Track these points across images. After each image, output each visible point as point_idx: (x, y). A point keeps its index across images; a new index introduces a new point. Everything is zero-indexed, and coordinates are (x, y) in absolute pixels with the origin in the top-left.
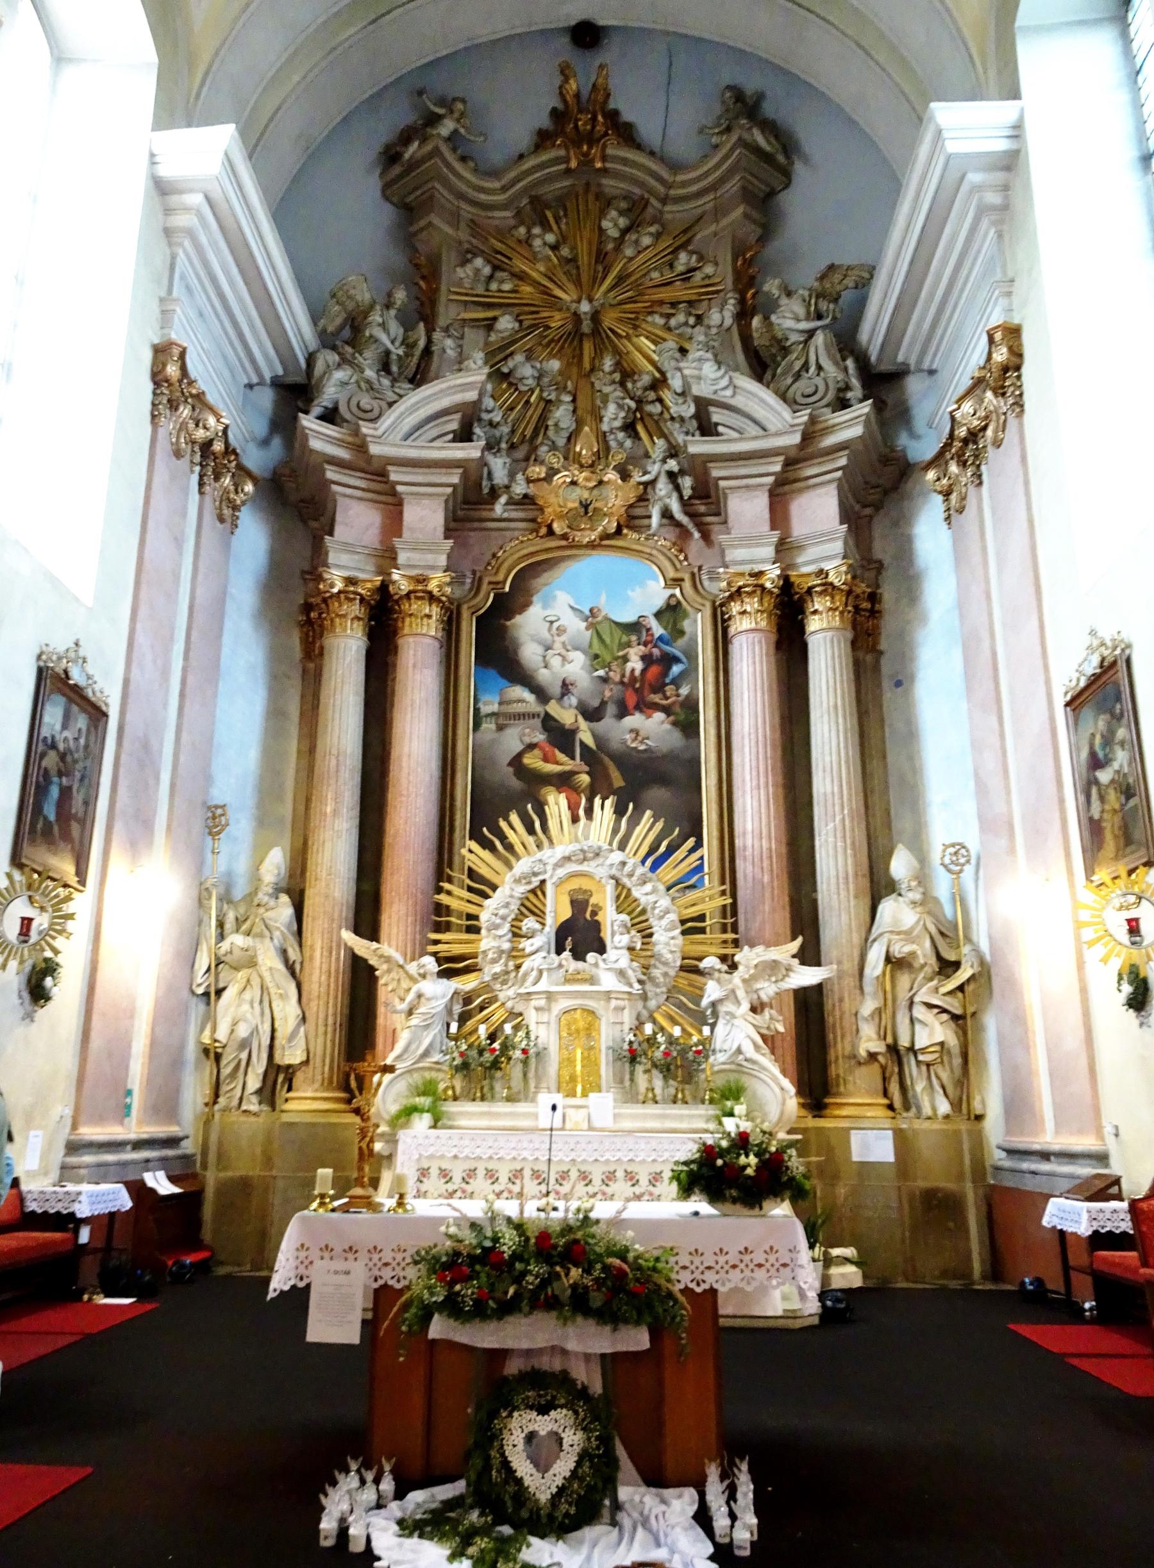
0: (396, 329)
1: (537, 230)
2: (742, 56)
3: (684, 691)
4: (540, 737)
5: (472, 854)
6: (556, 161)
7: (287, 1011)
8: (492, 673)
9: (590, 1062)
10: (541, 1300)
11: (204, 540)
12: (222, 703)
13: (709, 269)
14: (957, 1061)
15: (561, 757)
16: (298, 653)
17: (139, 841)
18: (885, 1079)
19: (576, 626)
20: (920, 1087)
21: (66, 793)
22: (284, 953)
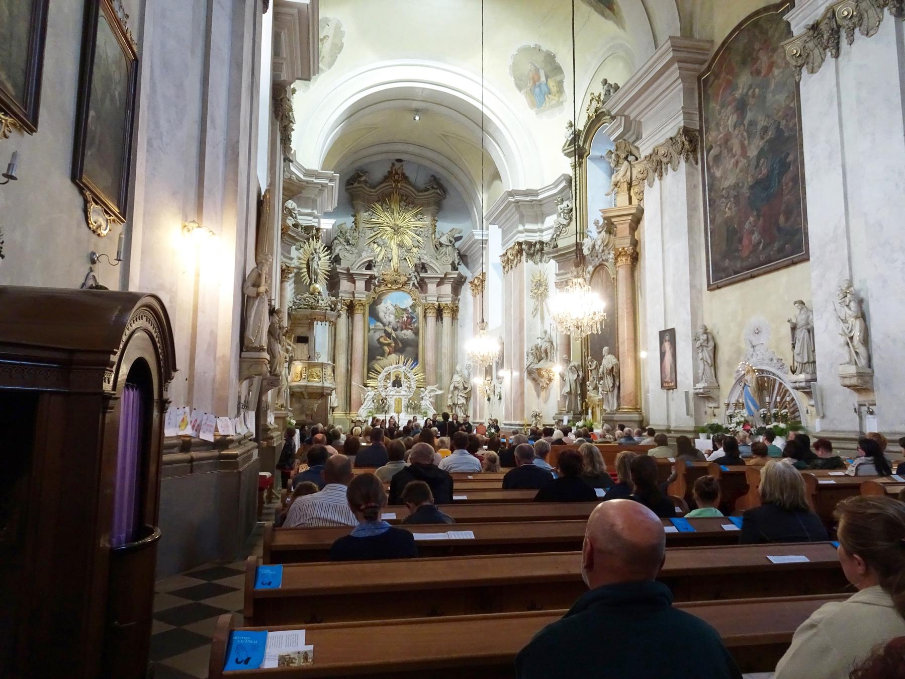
19: (392, 309)
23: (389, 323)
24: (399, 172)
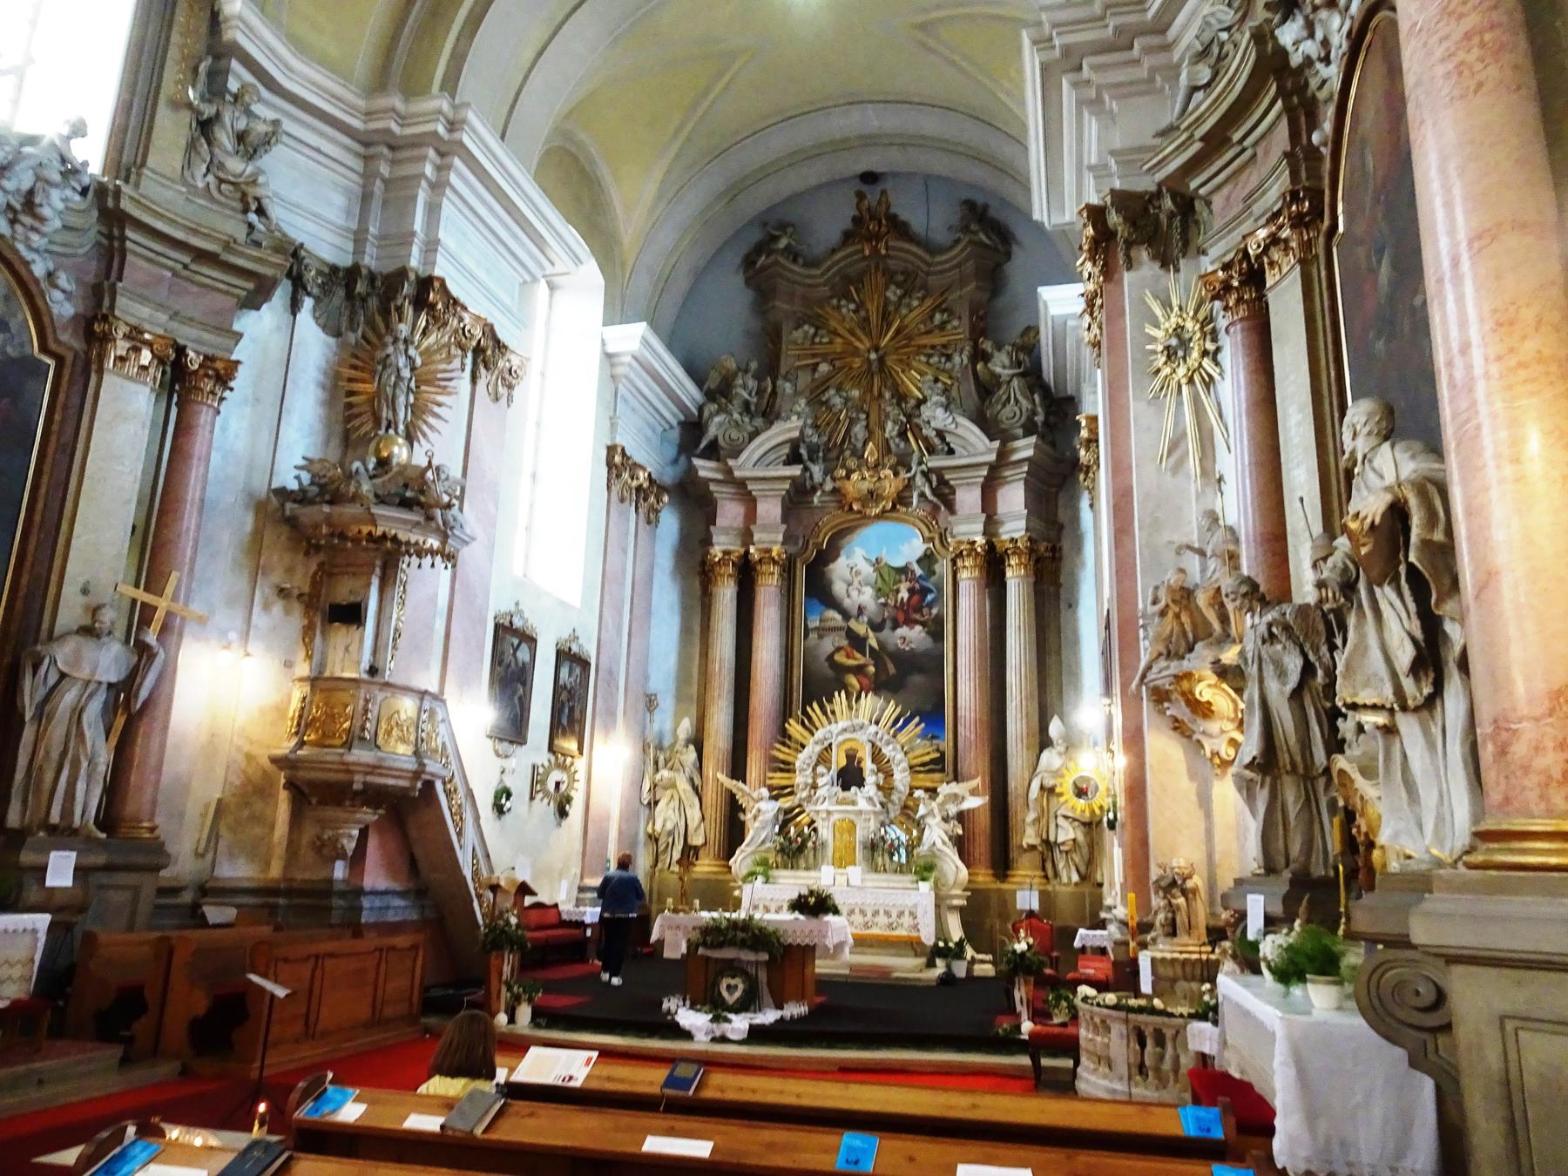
0: (752, 383)
1: (843, 302)
2: (972, 186)
3: (935, 611)
4: (845, 643)
6: (856, 252)
7: (694, 814)
8: (815, 601)
10: (732, 943)
11: (640, 543)
12: (654, 631)
13: (956, 323)
14: (1085, 850)
15: (858, 655)
16: (699, 593)
17: (609, 726)
18: (1044, 861)
19: (867, 570)
20: (1061, 865)
21: (572, 710)
22: (692, 780)
23: (861, 610)
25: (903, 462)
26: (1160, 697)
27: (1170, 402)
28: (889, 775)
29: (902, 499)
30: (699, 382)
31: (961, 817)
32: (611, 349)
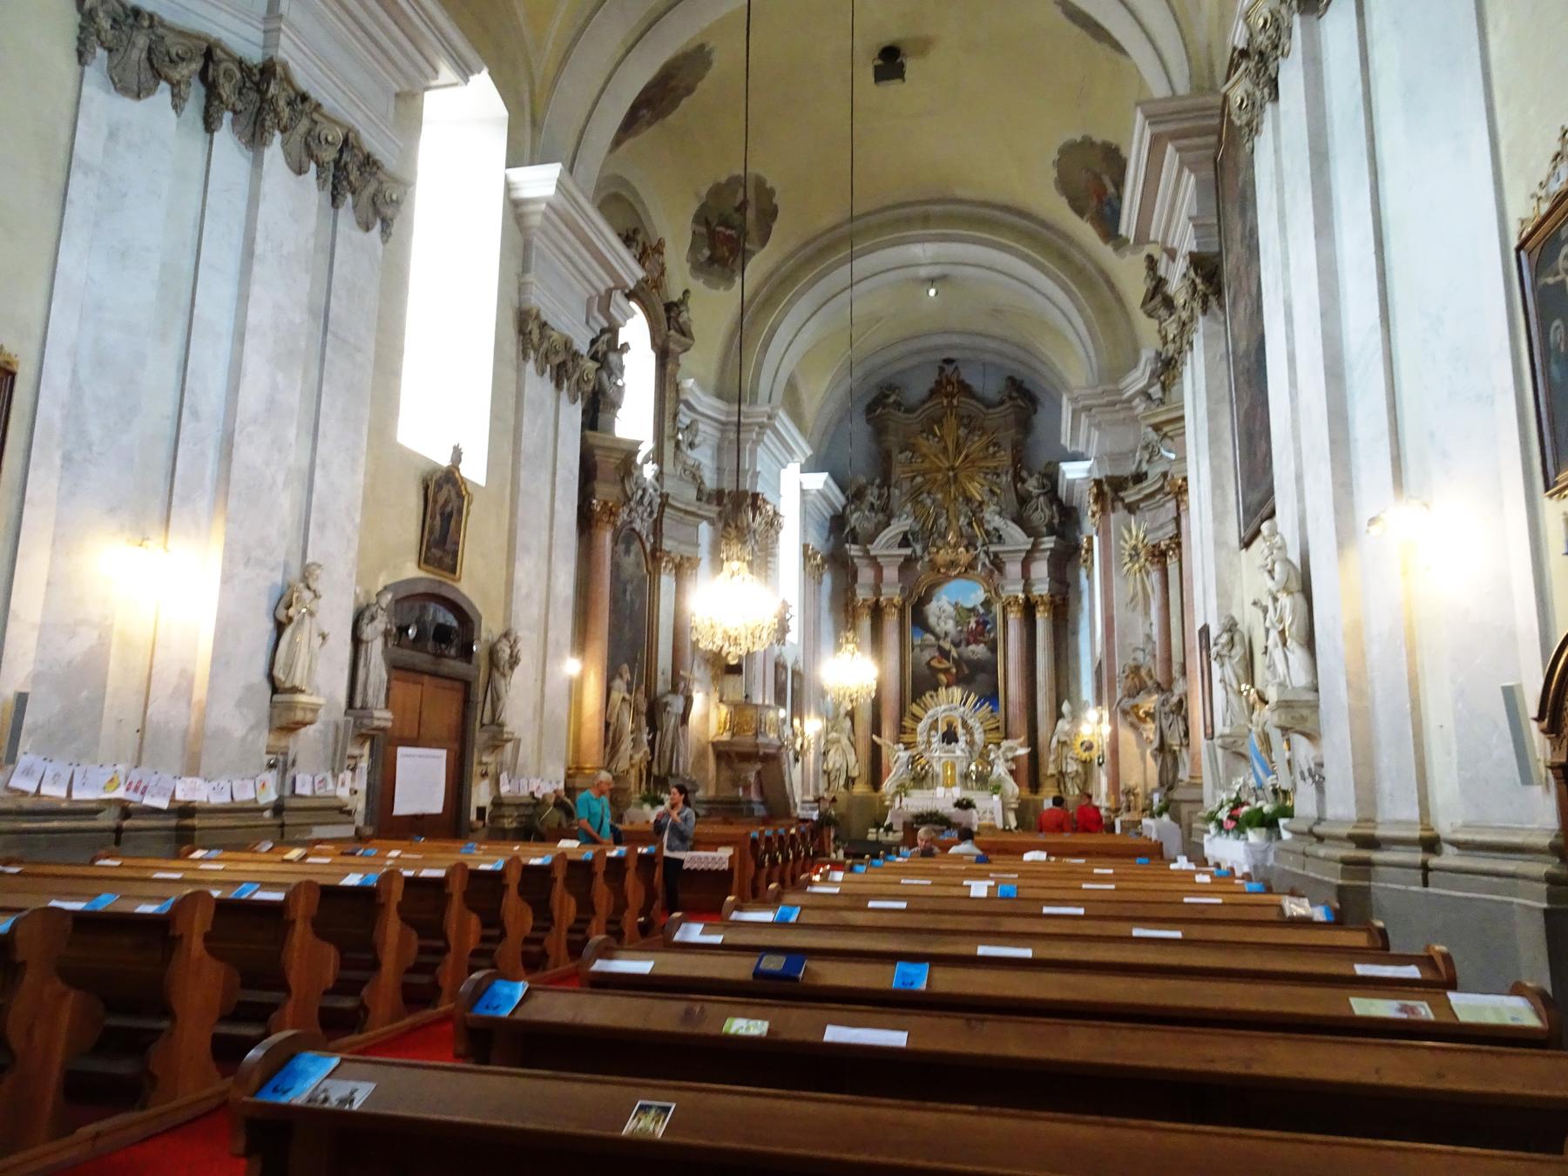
5: (915, 709)
7: (852, 758)
9: (953, 777)
19: (950, 610)
24: (954, 379)
25: (971, 544)
26: (1125, 713)
27: (1131, 578)
28: (972, 735)
29: (971, 566)
30: (843, 489)
31: (1014, 759)
32: (516, 195)
